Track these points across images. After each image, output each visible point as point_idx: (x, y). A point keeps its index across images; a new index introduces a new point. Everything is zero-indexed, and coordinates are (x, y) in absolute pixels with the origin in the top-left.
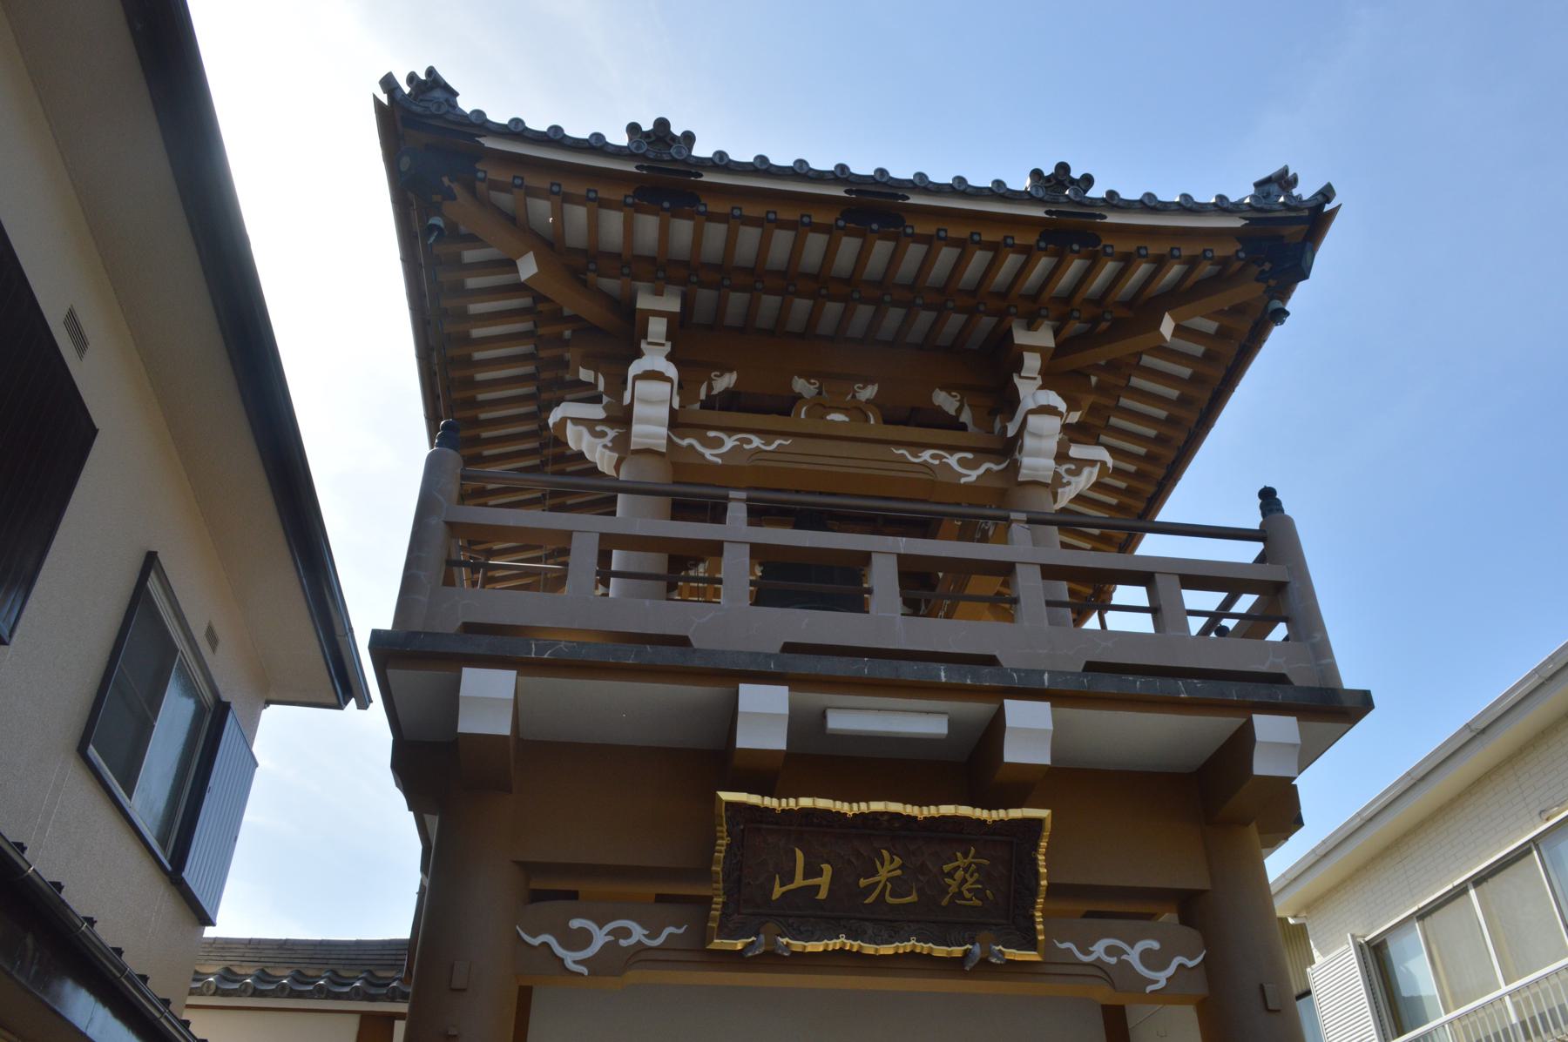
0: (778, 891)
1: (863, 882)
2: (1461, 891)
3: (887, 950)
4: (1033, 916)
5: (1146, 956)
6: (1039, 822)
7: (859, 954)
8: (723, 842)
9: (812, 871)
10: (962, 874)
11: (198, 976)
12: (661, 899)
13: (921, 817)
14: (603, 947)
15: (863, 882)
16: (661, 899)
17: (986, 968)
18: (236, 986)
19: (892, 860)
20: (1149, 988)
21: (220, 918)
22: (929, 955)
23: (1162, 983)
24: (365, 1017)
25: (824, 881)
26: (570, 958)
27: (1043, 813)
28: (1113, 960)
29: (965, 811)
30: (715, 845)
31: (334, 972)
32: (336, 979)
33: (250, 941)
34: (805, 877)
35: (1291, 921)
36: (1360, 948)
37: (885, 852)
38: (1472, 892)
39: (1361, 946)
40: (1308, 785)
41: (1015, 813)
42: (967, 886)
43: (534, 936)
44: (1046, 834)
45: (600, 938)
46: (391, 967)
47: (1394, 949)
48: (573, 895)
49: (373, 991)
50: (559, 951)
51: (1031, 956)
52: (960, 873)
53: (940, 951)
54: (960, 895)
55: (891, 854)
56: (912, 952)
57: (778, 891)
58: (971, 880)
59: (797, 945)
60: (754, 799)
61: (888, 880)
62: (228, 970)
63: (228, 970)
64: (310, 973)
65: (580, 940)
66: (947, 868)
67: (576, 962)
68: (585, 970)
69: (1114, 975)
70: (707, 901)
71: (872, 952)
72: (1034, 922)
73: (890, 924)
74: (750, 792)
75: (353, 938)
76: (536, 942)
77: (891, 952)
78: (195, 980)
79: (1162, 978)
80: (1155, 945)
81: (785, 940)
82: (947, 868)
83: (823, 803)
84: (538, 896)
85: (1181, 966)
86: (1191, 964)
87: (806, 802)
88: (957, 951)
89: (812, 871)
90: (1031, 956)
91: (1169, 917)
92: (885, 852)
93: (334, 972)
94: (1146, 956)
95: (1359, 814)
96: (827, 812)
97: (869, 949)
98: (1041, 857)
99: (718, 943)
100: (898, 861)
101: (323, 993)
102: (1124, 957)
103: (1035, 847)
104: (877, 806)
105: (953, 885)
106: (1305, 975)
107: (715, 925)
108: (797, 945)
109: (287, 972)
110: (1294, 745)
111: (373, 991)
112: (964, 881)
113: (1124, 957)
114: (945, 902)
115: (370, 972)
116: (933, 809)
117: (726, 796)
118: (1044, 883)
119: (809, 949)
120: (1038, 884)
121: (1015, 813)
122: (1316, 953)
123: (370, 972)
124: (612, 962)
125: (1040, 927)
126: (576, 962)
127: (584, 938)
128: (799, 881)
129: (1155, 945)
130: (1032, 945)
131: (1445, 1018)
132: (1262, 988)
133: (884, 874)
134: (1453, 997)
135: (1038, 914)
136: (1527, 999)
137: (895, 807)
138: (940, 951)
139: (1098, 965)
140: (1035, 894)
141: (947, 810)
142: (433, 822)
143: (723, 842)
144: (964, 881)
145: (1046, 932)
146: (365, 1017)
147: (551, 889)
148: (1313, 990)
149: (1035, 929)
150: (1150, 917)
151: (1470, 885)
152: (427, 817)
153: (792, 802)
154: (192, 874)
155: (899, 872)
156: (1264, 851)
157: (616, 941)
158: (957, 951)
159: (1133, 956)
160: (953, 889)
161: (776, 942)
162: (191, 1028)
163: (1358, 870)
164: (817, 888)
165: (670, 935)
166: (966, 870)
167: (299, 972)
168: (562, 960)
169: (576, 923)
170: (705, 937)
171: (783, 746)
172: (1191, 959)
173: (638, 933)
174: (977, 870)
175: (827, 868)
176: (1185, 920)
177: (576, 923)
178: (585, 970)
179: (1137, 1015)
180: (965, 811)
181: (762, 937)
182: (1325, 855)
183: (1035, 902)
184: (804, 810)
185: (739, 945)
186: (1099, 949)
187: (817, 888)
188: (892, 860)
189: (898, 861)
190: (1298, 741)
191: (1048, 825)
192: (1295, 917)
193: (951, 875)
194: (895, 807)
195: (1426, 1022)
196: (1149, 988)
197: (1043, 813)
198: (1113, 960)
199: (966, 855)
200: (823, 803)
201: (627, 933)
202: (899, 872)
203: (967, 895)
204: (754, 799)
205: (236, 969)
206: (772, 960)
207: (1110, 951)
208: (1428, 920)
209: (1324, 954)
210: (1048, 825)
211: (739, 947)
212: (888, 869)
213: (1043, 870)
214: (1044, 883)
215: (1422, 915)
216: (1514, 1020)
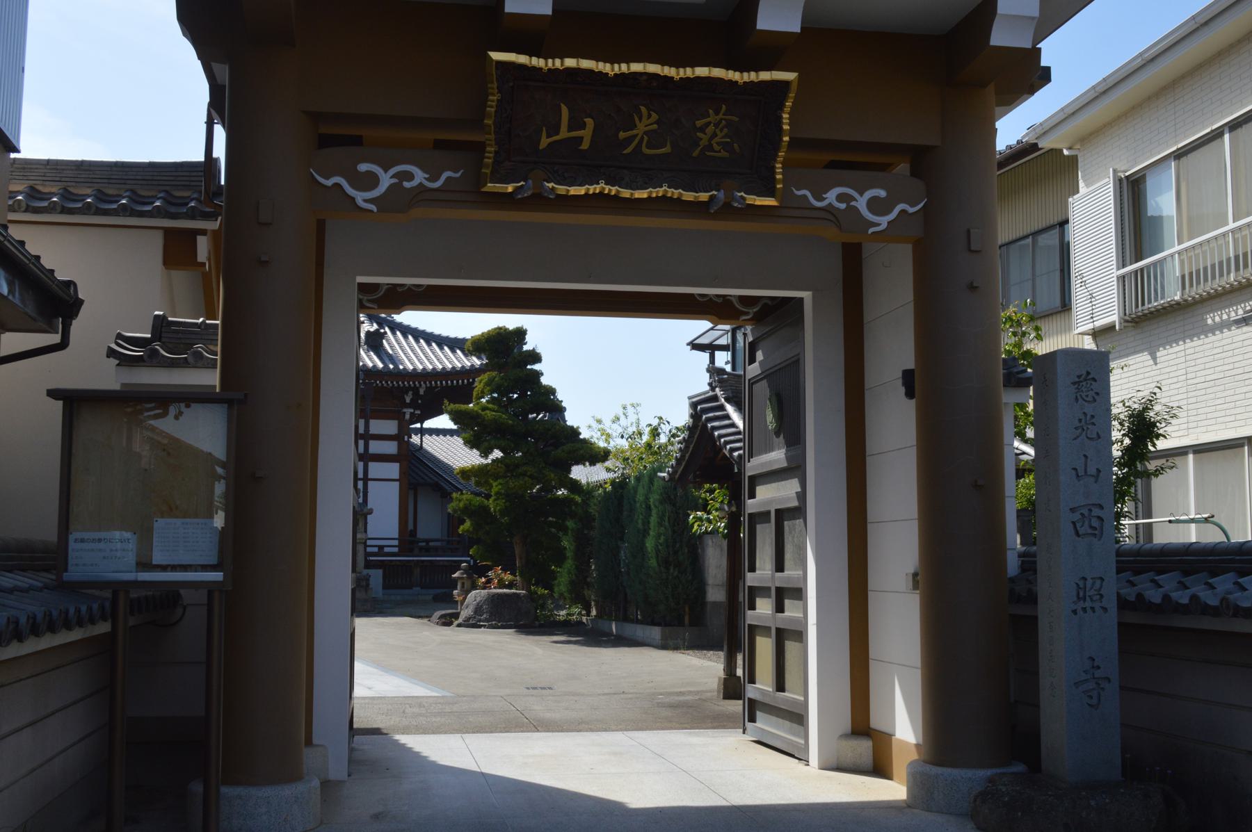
0: (545, 142)
1: (622, 135)
2: (1217, 135)
3: (642, 194)
4: (774, 167)
5: (874, 205)
6: (786, 84)
7: (616, 197)
8: (494, 99)
9: (576, 124)
10: (713, 130)
11: (12, 195)
12: (439, 145)
13: (677, 77)
14: (388, 189)
15: (622, 135)
16: (439, 145)
17: (728, 211)
18: (45, 204)
19: (649, 116)
20: (871, 230)
21: (23, 145)
22: (679, 200)
23: (884, 226)
24: (169, 233)
25: (587, 134)
26: (360, 197)
27: (790, 76)
28: (843, 206)
29: (718, 72)
30: (487, 100)
31: (133, 191)
32: (136, 198)
33: (48, 162)
34: (570, 129)
35: (1066, 152)
36: (1119, 182)
37: (643, 109)
38: (1227, 136)
39: (1121, 180)
40: (1052, 51)
41: (765, 76)
42: (717, 139)
43: (327, 178)
44: (792, 95)
45: (386, 180)
46: (187, 187)
47: (1151, 183)
48: (357, 141)
49: (173, 210)
50: (350, 191)
51: (770, 202)
52: (711, 128)
53: (689, 196)
54: (710, 147)
55: (649, 110)
56: (664, 196)
57: (545, 142)
58: (720, 134)
59: (561, 189)
60: (522, 59)
61: (646, 133)
62: (32, 188)
63: (32, 188)
64: (110, 192)
65: (370, 181)
66: (699, 123)
67: (365, 201)
68: (374, 208)
69: (844, 218)
70: (480, 147)
71: (628, 196)
72: (774, 173)
73: (645, 173)
74: (519, 52)
75: (146, 160)
76: (329, 183)
77: (645, 196)
78: (10, 198)
79: (883, 221)
80: (882, 193)
81: (550, 185)
82: (699, 123)
83: (586, 64)
84: (325, 142)
85: (903, 212)
86: (911, 210)
87: (570, 62)
88: (704, 196)
89: (576, 124)
90: (770, 202)
91: (903, 168)
92: (643, 109)
93: (133, 191)
94: (874, 205)
95: (1141, 54)
96: (591, 71)
97: (626, 193)
98: (785, 116)
99: (491, 187)
100: (655, 116)
101: (124, 211)
102: (853, 203)
103: (781, 107)
104: (636, 67)
105: (704, 139)
106: (1065, 207)
107: (488, 171)
108: (561, 189)
109: (89, 191)
110: (1033, 18)
111: (173, 210)
112: (715, 135)
113: (853, 203)
114: (695, 154)
115: (166, 192)
116: (689, 70)
117: (496, 56)
118: (786, 139)
119: (572, 193)
120: (781, 140)
121: (765, 76)
122: (1081, 184)
123: (166, 192)
124: (397, 201)
125: (779, 177)
126: (365, 201)
127: (372, 181)
128: (564, 134)
129: (882, 193)
130: (771, 193)
131: (1177, 248)
132: (968, 231)
133: (641, 128)
134: (1191, 226)
135: (779, 165)
136: (1244, 237)
137: (653, 68)
138: (689, 196)
139: (829, 209)
140: (777, 149)
141: (702, 71)
142: (223, 72)
143: (494, 99)
144: (715, 135)
145: (784, 181)
146: (169, 233)
147: (337, 137)
148: (1071, 221)
149: (774, 178)
150: (883, 167)
151: (1227, 129)
152: (216, 67)
153: (558, 62)
154: (876, 722)
155: (655, 126)
156: (998, 110)
157: (400, 183)
158: (704, 196)
159: (861, 203)
160: (704, 143)
161: (543, 186)
162: (27, 247)
163: (1119, 117)
164: (581, 139)
165: (448, 178)
166: (716, 125)
167: (99, 191)
168: (353, 199)
169: (363, 167)
170: (480, 181)
171: (549, 11)
172: (912, 206)
173: (420, 177)
174: (726, 126)
175: (589, 122)
176: (915, 173)
177: (363, 167)
178: (374, 208)
179: (868, 249)
180: (718, 72)
181: (530, 182)
182: (1104, 92)
183: (777, 156)
184: (568, 69)
185: (510, 188)
186: (831, 196)
187: (581, 139)
188: (649, 116)
189: (655, 116)
190: (1037, 14)
191: (794, 87)
192: (1070, 148)
193: (702, 130)
194: (653, 68)
195: (1163, 251)
196: (871, 230)
197: (790, 76)
198: (843, 206)
199: (717, 113)
200: (586, 64)
201: (410, 177)
202: (655, 126)
203: (716, 147)
204: (522, 59)
205: (40, 188)
206: (540, 201)
207: (840, 198)
208: (1184, 159)
209: (1087, 186)
210: (794, 87)
211: (510, 189)
212: (645, 123)
213: (786, 127)
214: (786, 139)
215: (1179, 155)
216: (1232, 255)
